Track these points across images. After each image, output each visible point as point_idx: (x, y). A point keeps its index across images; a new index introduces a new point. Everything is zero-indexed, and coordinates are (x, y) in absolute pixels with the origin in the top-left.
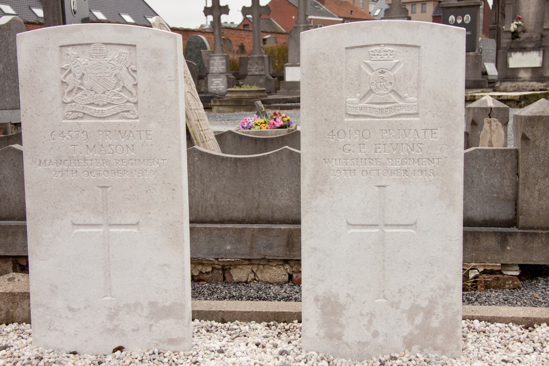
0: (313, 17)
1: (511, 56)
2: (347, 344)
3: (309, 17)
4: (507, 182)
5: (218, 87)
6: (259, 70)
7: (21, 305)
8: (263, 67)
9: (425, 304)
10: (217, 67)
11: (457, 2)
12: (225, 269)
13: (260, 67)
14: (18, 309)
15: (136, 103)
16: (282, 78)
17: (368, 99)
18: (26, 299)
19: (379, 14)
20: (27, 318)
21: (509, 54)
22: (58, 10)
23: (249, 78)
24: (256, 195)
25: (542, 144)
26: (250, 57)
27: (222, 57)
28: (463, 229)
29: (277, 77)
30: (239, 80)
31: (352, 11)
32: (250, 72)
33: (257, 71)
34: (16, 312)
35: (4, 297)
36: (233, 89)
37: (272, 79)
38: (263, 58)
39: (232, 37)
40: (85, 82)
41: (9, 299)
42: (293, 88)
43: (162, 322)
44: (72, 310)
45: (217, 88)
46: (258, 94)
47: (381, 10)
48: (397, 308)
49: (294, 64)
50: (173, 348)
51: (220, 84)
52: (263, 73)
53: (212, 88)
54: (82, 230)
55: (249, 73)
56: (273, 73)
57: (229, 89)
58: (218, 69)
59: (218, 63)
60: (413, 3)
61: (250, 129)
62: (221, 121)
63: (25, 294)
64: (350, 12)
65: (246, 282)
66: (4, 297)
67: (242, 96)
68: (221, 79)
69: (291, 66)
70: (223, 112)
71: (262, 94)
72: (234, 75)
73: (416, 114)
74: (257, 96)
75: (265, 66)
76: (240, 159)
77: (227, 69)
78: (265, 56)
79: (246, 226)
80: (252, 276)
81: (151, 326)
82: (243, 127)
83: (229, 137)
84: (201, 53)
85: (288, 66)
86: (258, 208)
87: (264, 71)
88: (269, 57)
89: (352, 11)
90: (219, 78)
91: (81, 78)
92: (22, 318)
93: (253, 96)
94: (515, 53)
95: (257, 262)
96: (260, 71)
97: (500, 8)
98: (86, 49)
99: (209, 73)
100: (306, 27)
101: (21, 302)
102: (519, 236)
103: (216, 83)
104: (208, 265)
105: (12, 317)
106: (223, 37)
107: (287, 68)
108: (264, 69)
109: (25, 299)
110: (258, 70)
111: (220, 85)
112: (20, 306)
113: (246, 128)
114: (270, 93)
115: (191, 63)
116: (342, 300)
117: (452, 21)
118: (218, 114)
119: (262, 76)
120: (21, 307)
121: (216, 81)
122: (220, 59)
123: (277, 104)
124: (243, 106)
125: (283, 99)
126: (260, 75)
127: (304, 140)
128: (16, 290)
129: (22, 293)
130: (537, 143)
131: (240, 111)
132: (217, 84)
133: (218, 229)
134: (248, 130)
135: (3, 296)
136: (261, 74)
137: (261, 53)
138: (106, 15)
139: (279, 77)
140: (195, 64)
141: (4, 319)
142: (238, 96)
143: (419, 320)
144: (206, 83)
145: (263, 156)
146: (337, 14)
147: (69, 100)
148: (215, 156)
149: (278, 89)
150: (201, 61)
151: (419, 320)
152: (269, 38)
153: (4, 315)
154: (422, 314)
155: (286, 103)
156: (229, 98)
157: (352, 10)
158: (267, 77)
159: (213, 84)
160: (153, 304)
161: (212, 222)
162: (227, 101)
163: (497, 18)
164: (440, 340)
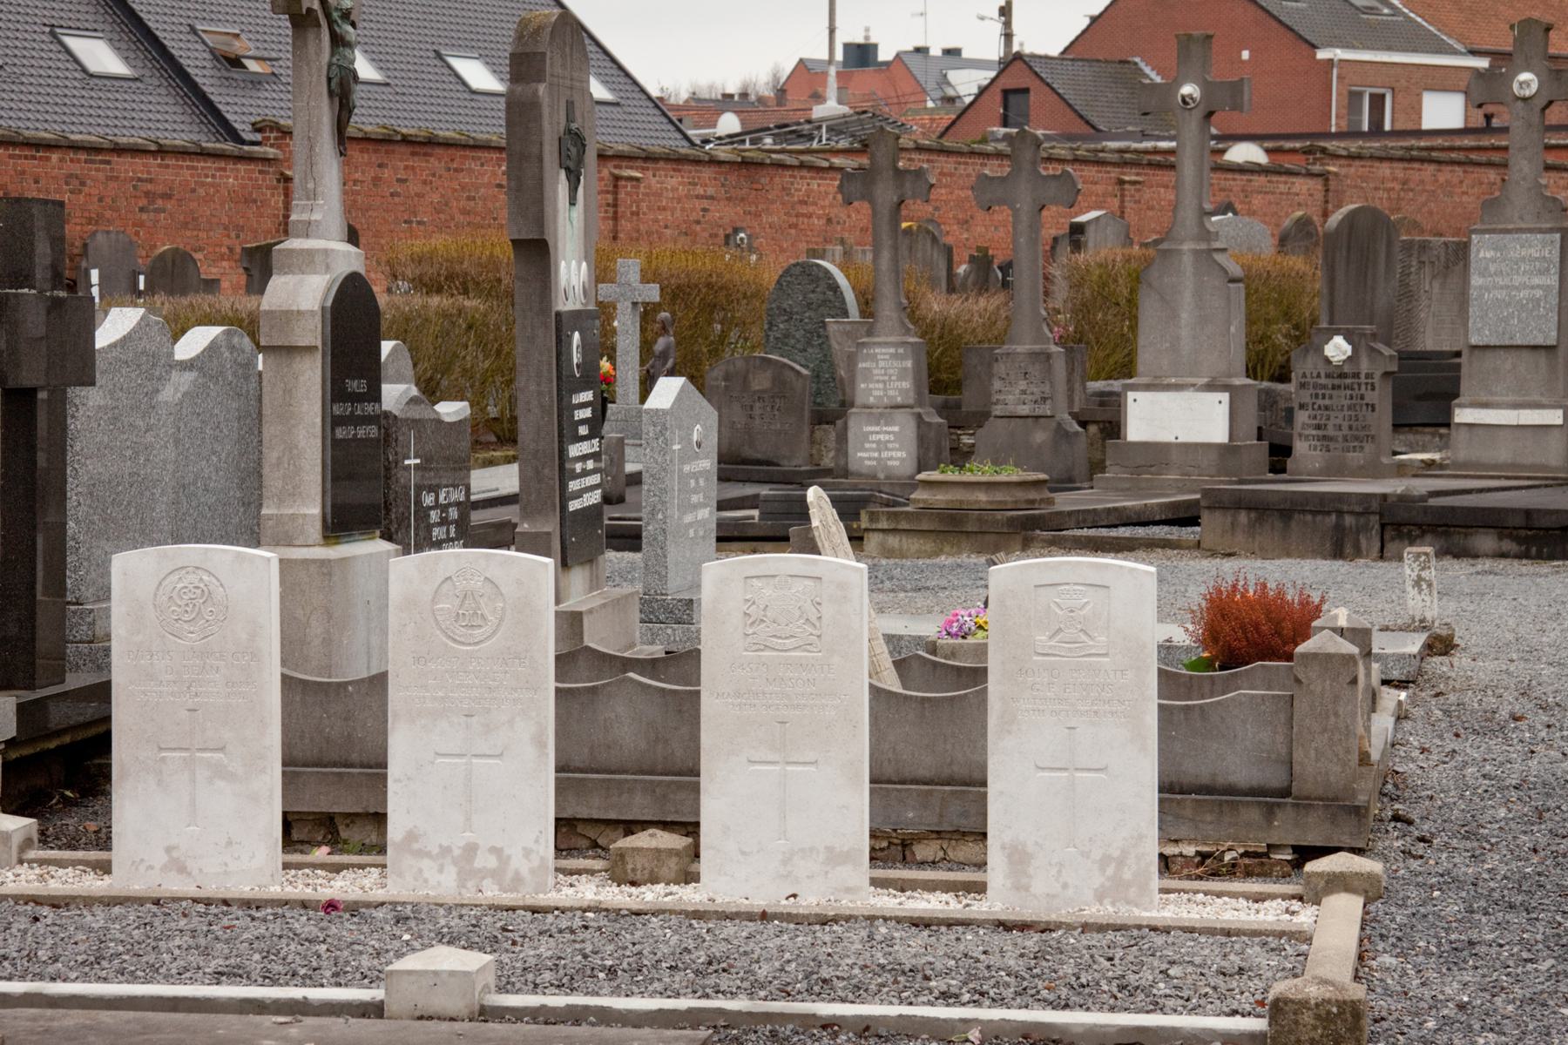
0: (1340, 54)
2: (1035, 896)
3: (1322, 55)
4: (1280, 738)
5: (885, 454)
6: (1034, 398)
9: (1116, 854)
10: (884, 382)
12: (905, 845)
15: (819, 636)
16: (1113, 428)
17: (1057, 638)
22: (550, 372)
23: (994, 430)
24: (949, 747)
25: (1319, 689)
27: (901, 351)
32: (999, 407)
36: (935, 475)
37: (1077, 433)
39: (946, 186)
40: (769, 614)
43: (839, 868)
44: (743, 853)
45: (878, 460)
46: (1021, 495)
48: (1088, 858)
50: (850, 897)
51: (890, 446)
52: (1046, 409)
53: (862, 459)
54: (758, 767)
55: (998, 410)
56: (1082, 410)
57: (923, 476)
58: (885, 390)
59: (886, 369)
61: (963, 637)
62: (893, 591)
65: (934, 862)
67: (968, 502)
68: (896, 429)
69: (1148, 387)
71: (1033, 495)
72: (943, 409)
73: (1105, 655)
74: (1016, 502)
76: (929, 699)
77: (919, 393)
80: (941, 854)
81: (827, 873)
82: (949, 634)
83: (915, 664)
84: (824, 325)
86: (951, 764)
87: (1048, 402)
90: (887, 424)
91: (764, 610)
93: (1005, 502)
95: (948, 836)
98: (772, 581)
99: (852, 405)
100: (1202, 251)
102: (1289, 808)
103: (879, 442)
104: (883, 838)
106: (904, 225)
107: (1131, 395)
111: (892, 450)
113: (957, 635)
114: (1066, 482)
115: (792, 369)
118: (884, 562)
119: (1042, 420)
121: (877, 433)
122: (895, 356)
123: (1085, 532)
126: (1037, 417)
127: (991, 677)
128: (662, 846)
130: (1312, 687)
131: (959, 553)
132: (882, 446)
133: (897, 790)
134: (960, 641)
136: (1038, 412)
138: (374, 60)
139: (1104, 422)
140: (805, 372)
143: (1110, 871)
144: (842, 439)
145: (959, 696)
147: (751, 631)
148: (895, 693)
149: (1097, 466)
150: (825, 356)
151: (1110, 871)
154: (1113, 865)
155: (1116, 526)
159: (867, 446)
160: (829, 849)
161: (889, 782)
164: (1133, 892)
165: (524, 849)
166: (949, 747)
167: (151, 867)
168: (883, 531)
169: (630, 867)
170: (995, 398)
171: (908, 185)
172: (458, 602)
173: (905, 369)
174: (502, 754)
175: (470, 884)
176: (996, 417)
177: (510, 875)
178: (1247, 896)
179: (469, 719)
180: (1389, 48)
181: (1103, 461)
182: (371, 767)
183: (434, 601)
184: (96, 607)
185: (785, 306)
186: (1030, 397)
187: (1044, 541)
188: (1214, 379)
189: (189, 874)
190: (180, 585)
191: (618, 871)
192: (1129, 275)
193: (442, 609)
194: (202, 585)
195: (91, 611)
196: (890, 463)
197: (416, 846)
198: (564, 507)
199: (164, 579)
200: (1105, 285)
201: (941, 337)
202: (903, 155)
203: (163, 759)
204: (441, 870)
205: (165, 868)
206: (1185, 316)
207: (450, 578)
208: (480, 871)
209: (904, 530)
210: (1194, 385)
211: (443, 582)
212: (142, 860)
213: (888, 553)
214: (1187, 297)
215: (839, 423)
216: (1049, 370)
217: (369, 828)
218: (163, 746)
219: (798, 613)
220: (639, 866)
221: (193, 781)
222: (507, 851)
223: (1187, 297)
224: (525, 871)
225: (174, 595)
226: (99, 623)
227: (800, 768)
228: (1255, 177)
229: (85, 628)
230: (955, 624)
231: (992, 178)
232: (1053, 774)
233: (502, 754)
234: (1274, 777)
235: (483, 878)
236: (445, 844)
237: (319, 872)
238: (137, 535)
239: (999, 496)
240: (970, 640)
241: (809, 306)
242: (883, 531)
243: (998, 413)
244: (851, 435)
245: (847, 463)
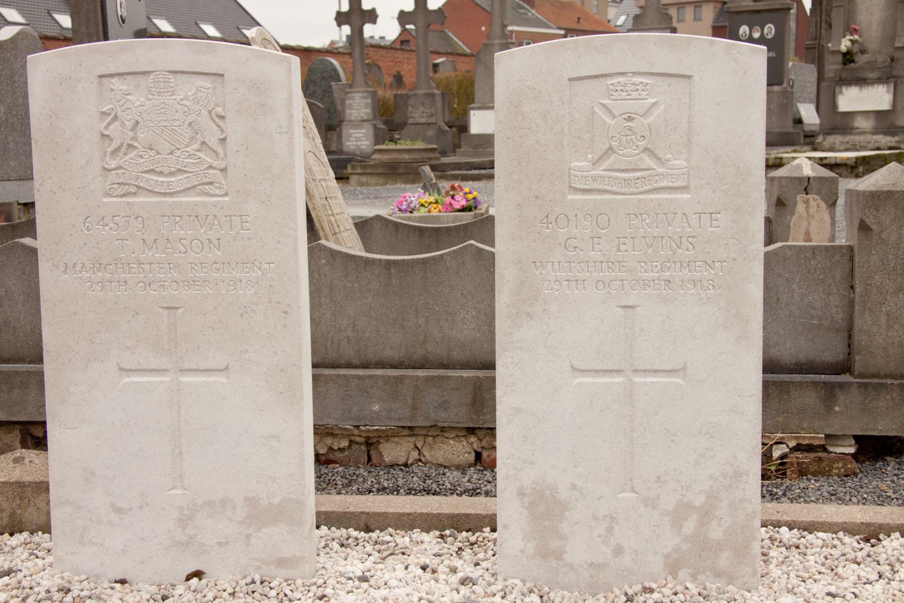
0: (515, 28)
1: (841, 92)
2: (571, 566)
3: (509, 28)
4: (834, 301)
5: (359, 143)
7: (35, 503)
8: (433, 110)
9: (699, 501)
10: (358, 110)
12: (370, 443)
13: (428, 111)
14: (30, 510)
15: (224, 170)
16: (464, 128)
17: (606, 164)
19: (624, 23)
21: (837, 89)
23: (409, 129)
24: (422, 321)
25: (893, 238)
27: (365, 95)
28: (763, 377)
29: (456, 126)
31: (579, 19)
33: (423, 117)
34: (27, 514)
35: (6, 489)
36: (383, 147)
37: (447, 131)
38: (433, 95)
40: (141, 136)
41: (15, 493)
42: (482, 145)
44: (118, 510)
45: (357, 146)
46: (425, 155)
47: (627, 17)
49: (484, 105)
52: (433, 120)
53: (349, 146)
54: (135, 379)
55: (411, 121)
57: (377, 147)
58: (359, 113)
61: (411, 212)
62: (363, 199)
63: (41, 485)
64: (577, 20)
69: (480, 108)
70: (368, 185)
71: (431, 155)
72: (385, 123)
73: (685, 189)
74: (422, 159)
76: (395, 262)
77: (374, 114)
78: (436, 92)
79: (405, 372)
80: (415, 455)
81: (248, 537)
82: (400, 210)
83: (377, 226)
84: (330, 87)
85: (473, 109)
86: (424, 342)
87: (434, 116)
88: (443, 94)
89: (579, 19)
90: (360, 129)
91: (134, 129)
92: (36, 524)
93: (417, 159)
94: (849, 88)
95: (424, 432)
96: (428, 117)
97: (824, 13)
98: (143, 81)
99: (344, 121)
100: (504, 44)
101: (35, 498)
102: (854, 389)
103: (356, 138)
104: (343, 436)
105: (20, 522)
106: (367, 61)
107: (472, 112)
108: (435, 114)
109: (41, 493)
110: (425, 115)
112: (33, 504)
113: (406, 211)
114: (444, 153)
115: (315, 104)
116: (563, 494)
117: (744, 35)
118: (359, 188)
119: (431, 125)
120: (34, 506)
121: (356, 133)
122: (363, 98)
123: (457, 172)
124: (400, 174)
125: (466, 163)
126: (429, 124)
129: (36, 483)
130: (884, 235)
131: (396, 183)
132: (358, 139)
133: (359, 377)
135: (5, 487)
138: (171, 22)
140: (321, 106)
141: (6, 525)
143: (689, 527)
144: (340, 136)
145: (434, 258)
146: (555, 24)
147: (113, 164)
148: (353, 256)
149: (458, 146)
151: (689, 527)
152: (443, 62)
153: (7, 519)
156: (377, 161)
157: (579, 16)
158: (440, 129)
159: (351, 139)
160: (251, 501)
161: (349, 366)
162: (375, 166)
163: (818, 30)
164: (724, 560)
166: (422, 321)
168: (359, 174)
170: (410, 115)
173: (368, 103)
176: (410, 124)
178: (850, 529)
180: (532, 26)
181: (460, 144)
185: (313, 79)
196: (363, 147)
200: (448, 85)
201: (383, 106)
202: (367, 48)
213: (361, 184)
215: (338, 129)
219: (188, 133)
227: (201, 379)
230: (405, 203)
232: (598, 380)
234: (832, 352)
239: (414, 156)
240: (416, 214)
241: (324, 78)
242: (359, 174)
243: (411, 122)
244: (344, 135)
245: (342, 148)
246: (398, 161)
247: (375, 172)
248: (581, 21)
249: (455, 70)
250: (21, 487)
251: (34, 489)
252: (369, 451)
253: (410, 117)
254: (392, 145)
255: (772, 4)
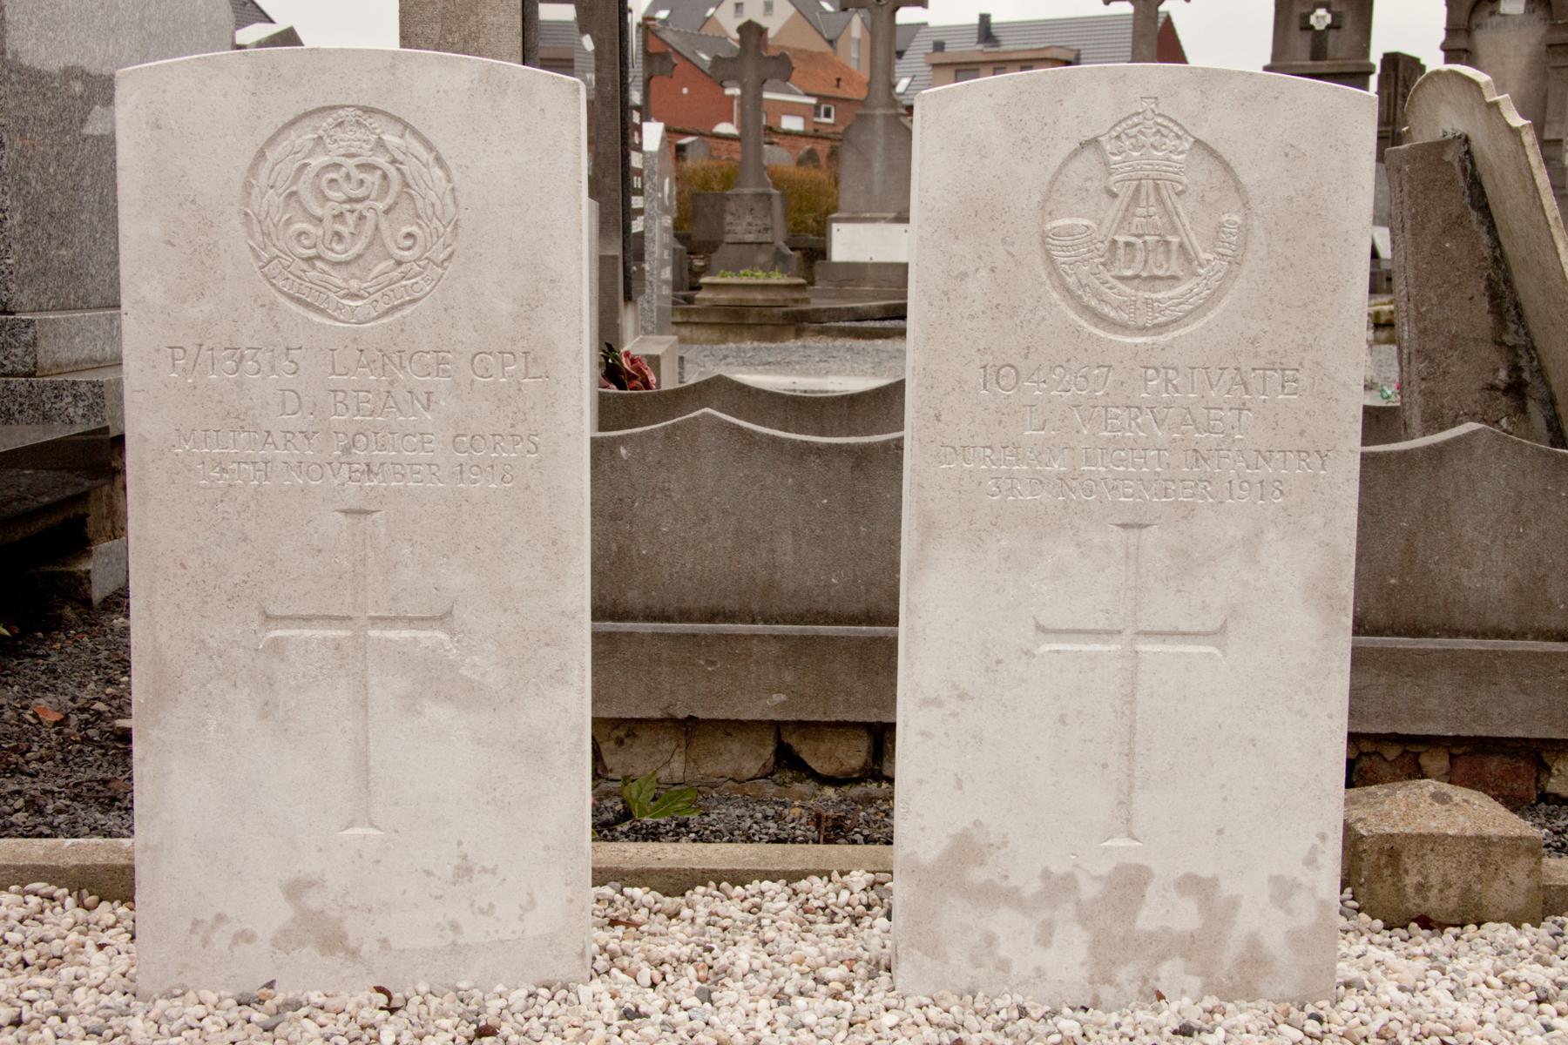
6: (758, 228)
11: (1309, 63)
13: (759, 222)
14: (1496, 885)
16: (815, 254)
18: (1522, 857)
19: (906, 90)
20: (1520, 911)
26: (733, 195)
28: (1353, 641)
29: (800, 249)
30: (692, 257)
31: (839, 80)
32: (730, 236)
33: (750, 233)
35: (1458, 849)
38: (769, 196)
41: (1474, 856)
42: (852, 280)
47: (912, 80)
49: (855, 216)
52: (767, 237)
55: (729, 238)
60: (997, 65)
63: (1520, 842)
64: (835, 82)
66: (1458, 849)
67: (748, 300)
71: (796, 295)
74: (785, 300)
75: (772, 219)
79: (1482, 644)
85: (838, 220)
87: (769, 232)
88: (783, 195)
89: (839, 80)
92: (1506, 910)
93: (776, 301)
96: (759, 232)
97: (1400, 84)
100: (892, 115)
101: (1508, 865)
105: (1478, 906)
107: (835, 226)
109: (1518, 856)
112: (1503, 875)
119: (764, 246)
120: (1504, 879)
124: (749, 325)
129: (1511, 838)
131: (742, 340)
136: (761, 240)
137: (762, 183)
139: (805, 249)
141: (1454, 911)
142: (734, 300)
146: (800, 87)
152: (693, 143)
153: (1456, 899)
156: (707, 303)
157: (838, 76)
158: (778, 250)
163: (1392, 111)
165: (1276, 880)
167: (246, 937)
169: (1411, 880)
170: (727, 228)
171: (657, 64)
172: (1114, 210)
174: (1222, 631)
175: (1123, 974)
176: (728, 243)
177: (1234, 947)
179: (1133, 535)
182: (668, 619)
183: (1047, 208)
184: (37, 317)
186: (754, 228)
187: (814, 331)
188: (899, 213)
189: (354, 953)
190: (318, 161)
191: (1383, 891)
192: (723, 175)
193: (1069, 232)
194: (382, 161)
195: (30, 324)
197: (977, 875)
198: (626, 228)
199: (272, 140)
203: (277, 646)
204: (1045, 937)
205: (285, 940)
206: (877, 166)
207: (1094, 142)
208: (1151, 938)
209: (697, 323)
210: (884, 218)
211: (1075, 154)
212: (220, 918)
214: (879, 149)
216: (769, 209)
217: (667, 746)
218: (275, 610)
220: (1435, 879)
221: (363, 705)
222: (1228, 888)
223: (879, 149)
224: (1274, 941)
225: (303, 187)
226: (42, 343)
228: (733, 143)
229: (19, 352)
231: (725, 59)
233: (1222, 631)
235: (1163, 957)
236: (1058, 868)
237: (637, 892)
238: (95, 219)
239: (772, 295)
243: (729, 241)
246: (744, 304)
247: (707, 321)
248: (841, 84)
249: (711, 157)
250: (1484, 845)
251: (1507, 850)
252: (607, 779)
253: (728, 233)
254: (732, 276)
255: (1344, 65)
